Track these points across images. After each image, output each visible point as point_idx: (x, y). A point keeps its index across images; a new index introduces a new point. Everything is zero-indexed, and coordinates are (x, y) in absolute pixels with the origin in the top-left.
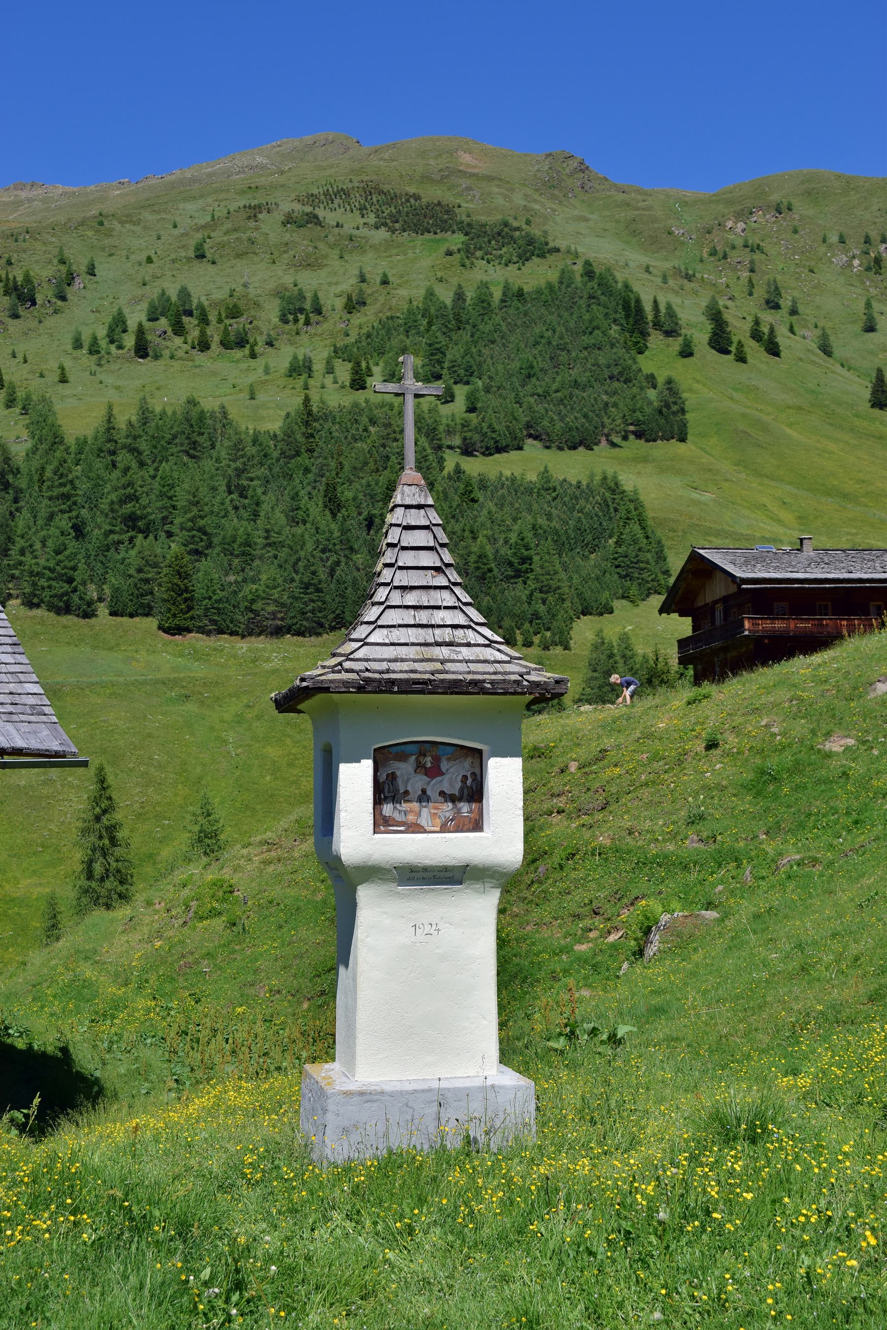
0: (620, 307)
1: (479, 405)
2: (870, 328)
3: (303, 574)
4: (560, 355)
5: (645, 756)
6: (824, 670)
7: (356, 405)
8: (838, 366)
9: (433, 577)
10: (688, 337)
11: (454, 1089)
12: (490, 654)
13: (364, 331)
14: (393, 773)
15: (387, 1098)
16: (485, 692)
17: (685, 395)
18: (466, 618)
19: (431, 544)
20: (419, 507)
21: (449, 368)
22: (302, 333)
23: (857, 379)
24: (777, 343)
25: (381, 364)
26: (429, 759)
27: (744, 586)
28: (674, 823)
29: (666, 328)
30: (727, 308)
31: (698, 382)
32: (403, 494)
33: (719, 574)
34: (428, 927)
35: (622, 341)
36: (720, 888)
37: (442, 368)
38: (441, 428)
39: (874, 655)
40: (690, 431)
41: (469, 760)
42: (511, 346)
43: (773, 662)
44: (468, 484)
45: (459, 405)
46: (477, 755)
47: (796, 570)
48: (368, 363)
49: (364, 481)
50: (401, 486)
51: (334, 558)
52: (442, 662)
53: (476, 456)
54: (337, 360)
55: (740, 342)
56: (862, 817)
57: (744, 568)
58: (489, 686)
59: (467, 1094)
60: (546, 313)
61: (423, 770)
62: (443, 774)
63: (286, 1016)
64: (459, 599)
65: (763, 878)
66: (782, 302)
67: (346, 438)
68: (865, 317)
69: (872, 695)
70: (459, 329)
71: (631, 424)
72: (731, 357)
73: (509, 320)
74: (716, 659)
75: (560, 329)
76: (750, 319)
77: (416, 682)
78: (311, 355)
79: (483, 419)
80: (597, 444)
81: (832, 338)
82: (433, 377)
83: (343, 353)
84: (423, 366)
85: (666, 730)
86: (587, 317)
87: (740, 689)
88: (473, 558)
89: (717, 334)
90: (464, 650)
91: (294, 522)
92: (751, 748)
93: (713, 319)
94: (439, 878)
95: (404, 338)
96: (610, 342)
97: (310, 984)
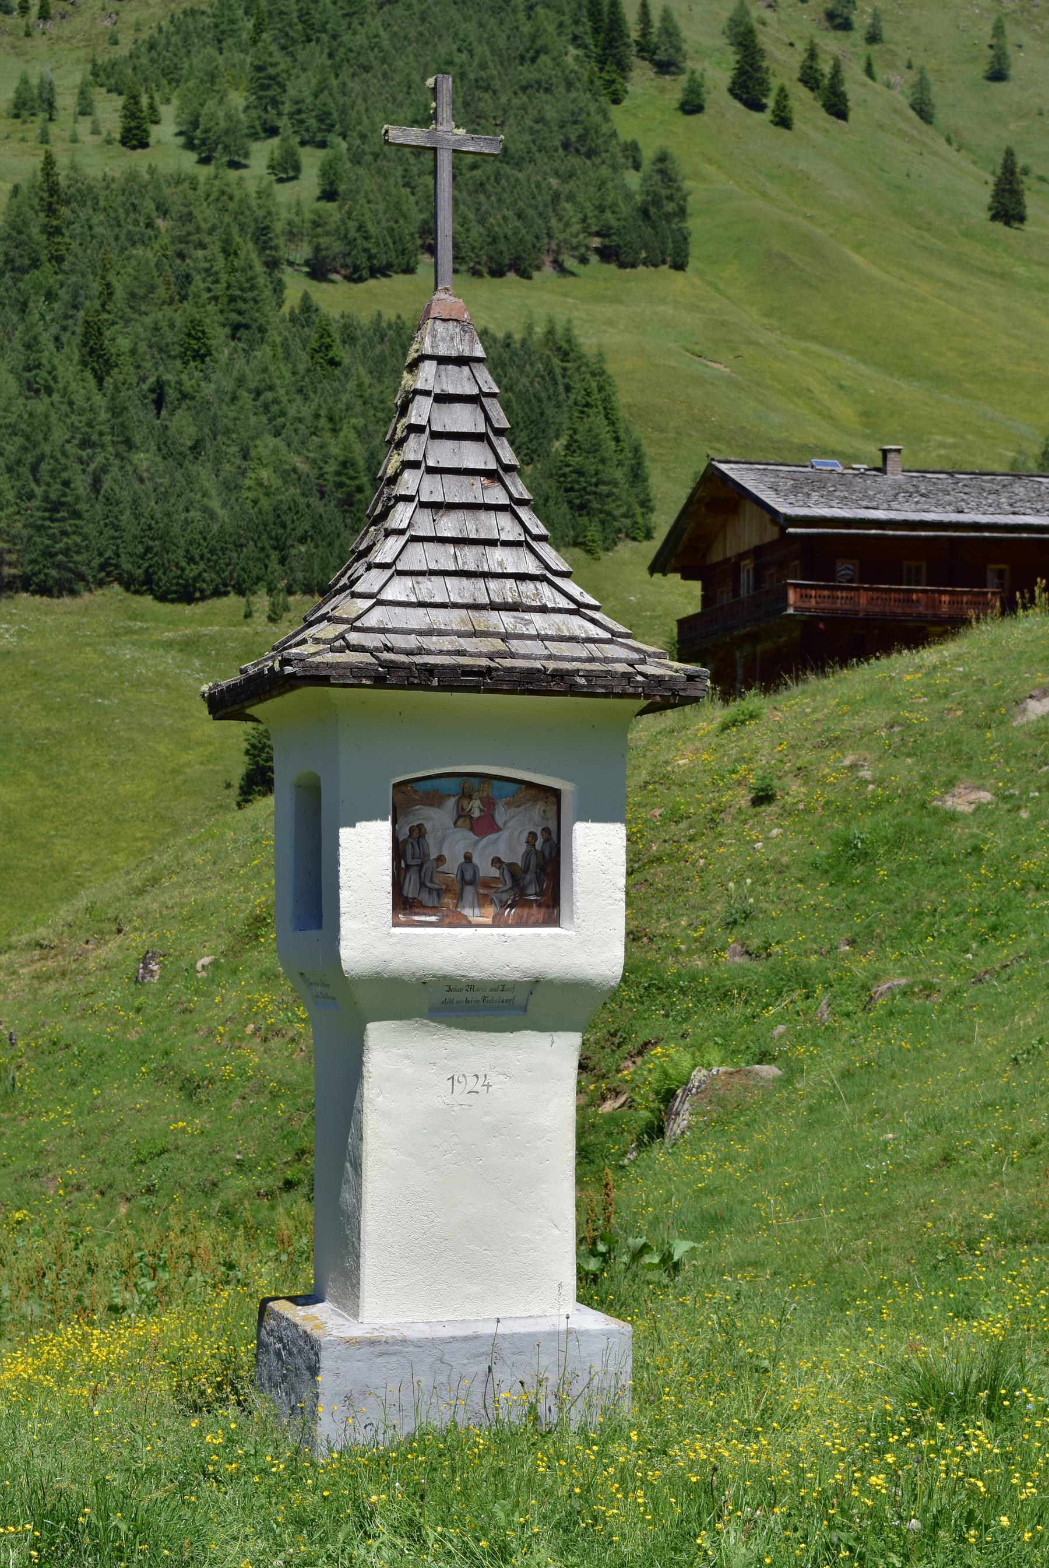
0: (585, 12)
1: (342, 188)
2: (998, 75)
3: (48, 485)
4: (480, 99)
5: (657, 812)
6: (943, 676)
7: (132, 176)
8: (942, 141)
9: (484, 488)
10: (697, 75)
11: (512, 1335)
12: (577, 625)
13: (145, 35)
14: (420, 827)
15: (412, 1349)
16: (574, 691)
17: (688, 185)
18: (537, 563)
19: (481, 428)
20: (461, 361)
21: (291, 115)
22: (36, 34)
23: (972, 168)
24: (844, 95)
25: (175, 101)
26: (476, 803)
27: (791, 530)
28: (705, 924)
29: (661, 56)
30: (764, 24)
31: (710, 161)
32: (434, 336)
33: (749, 507)
34: (471, 1082)
35: (585, 78)
36: (781, 1028)
37: (280, 114)
38: (279, 226)
39: (1022, 653)
40: (695, 250)
41: (540, 806)
42: (398, 78)
43: (859, 660)
44: (325, 333)
45: (309, 182)
46: (553, 799)
47: (874, 504)
48: (151, 97)
49: (148, 320)
50: (430, 322)
51: (100, 459)
52: (505, 637)
53: (332, 281)
54: (98, 89)
55: (782, 89)
56: (1004, 920)
57: (792, 498)
58: (582, 681)
59: (533, 1343)
60: (458, 17)
61: (468, 821)
62: (498, 829)
63: (93, 1226)
64: (526, 530)
65: (848, 1015)
66: (855, 18)
67: (117, 238)
68: (992, 52)
69: (1020, 720)
70: (309, 40)
71: (598, 234)
72: (767, 116)
73: (396, 28)
74: (738, 654)
75: (482, 50)
76: (801, 46)
77: (468, 671)
78: (53, 77)
79: (349, 213)
80: (538, 268)
81: (935, 89)
82: (265, 130)
83: (108, 78)
84: (247, 107)
85: (690, 770)
86: (526, 29)
87: (808, 704)
88: (331, 468)
89: (745, 73)
90: (536, 617)
91: (32, 389)
92: (827, 803)
93: (740, 44)
94: (492, 1001)
95: (215, 53)
96: (566, 79)
97: (129, 1176)
